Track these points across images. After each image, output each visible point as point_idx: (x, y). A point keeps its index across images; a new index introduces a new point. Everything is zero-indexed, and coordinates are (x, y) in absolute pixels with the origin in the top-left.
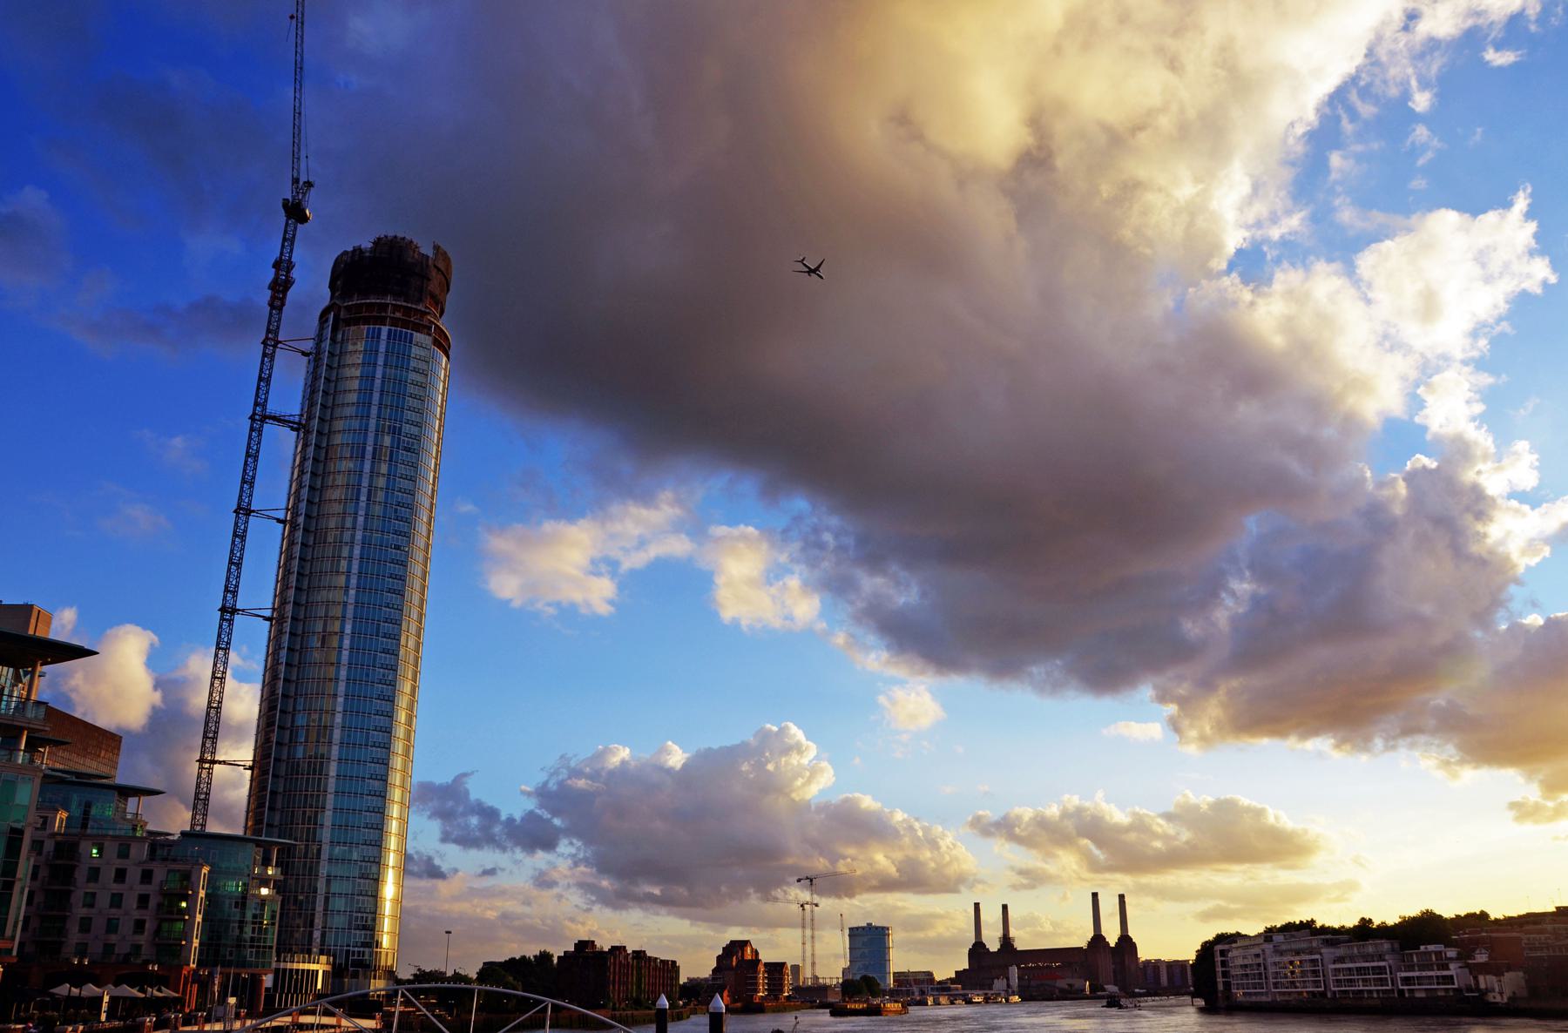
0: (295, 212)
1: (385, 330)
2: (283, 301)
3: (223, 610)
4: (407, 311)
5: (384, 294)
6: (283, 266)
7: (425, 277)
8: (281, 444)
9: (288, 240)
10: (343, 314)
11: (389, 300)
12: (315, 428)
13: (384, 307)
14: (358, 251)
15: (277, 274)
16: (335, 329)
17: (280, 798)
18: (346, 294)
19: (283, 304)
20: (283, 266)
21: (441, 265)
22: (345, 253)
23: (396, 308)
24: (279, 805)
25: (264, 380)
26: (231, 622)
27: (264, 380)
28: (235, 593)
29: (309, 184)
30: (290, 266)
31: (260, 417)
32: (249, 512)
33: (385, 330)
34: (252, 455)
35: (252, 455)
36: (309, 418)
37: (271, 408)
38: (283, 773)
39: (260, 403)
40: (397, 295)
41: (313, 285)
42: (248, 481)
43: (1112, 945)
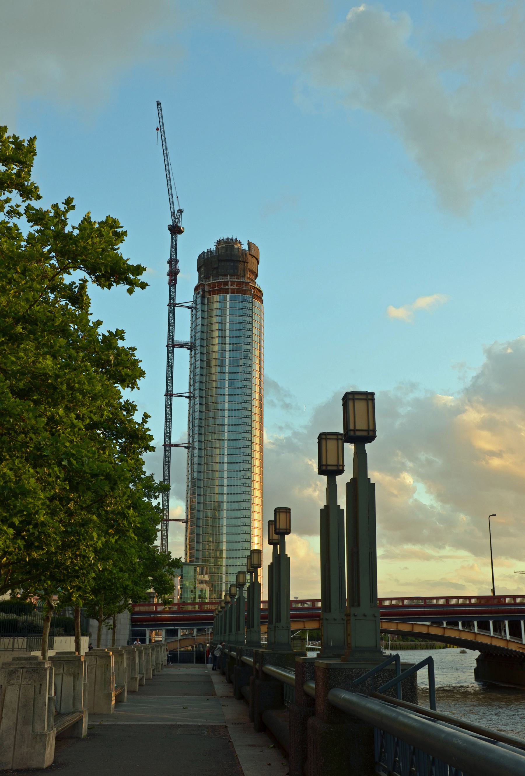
0: (175, 230)
1: (228, 296)
2: (175, 280)
3: (165, 445)
4: (238, 283)
5: (225, 275)
6: (173, 262)
7: (245, 262)
8: (182, 356)
9: (174, 247)
10: (207, 289)
11: (228, 279)
12: (201, 347)
13: (226, 283)
14: (209, 251)
15: (170, 267)
16: (203, 297)
17: (201, 537)
18: (207, 277)
19: (176, 283)
20: (173, 262)
21: (253, 253)
22: (204, 253)
23: (233, 283)
24: (201, 541)
25: (171, 325)
26: (171, 400)
27: (171, 325)
28: (170, 437)
29: (180, 211)
30: (176, 262)
31: (172, 345)
32: (172, 395)
33: (228, 296)
34: (170, 366)
35: (170, 366)
36: (193, 441)
37: (173, 441)
38: (201, 525)
39: (171, 337)
40: (232, 275)
41: (189, 278)
42: (170, 379)
43: (427, 666)
